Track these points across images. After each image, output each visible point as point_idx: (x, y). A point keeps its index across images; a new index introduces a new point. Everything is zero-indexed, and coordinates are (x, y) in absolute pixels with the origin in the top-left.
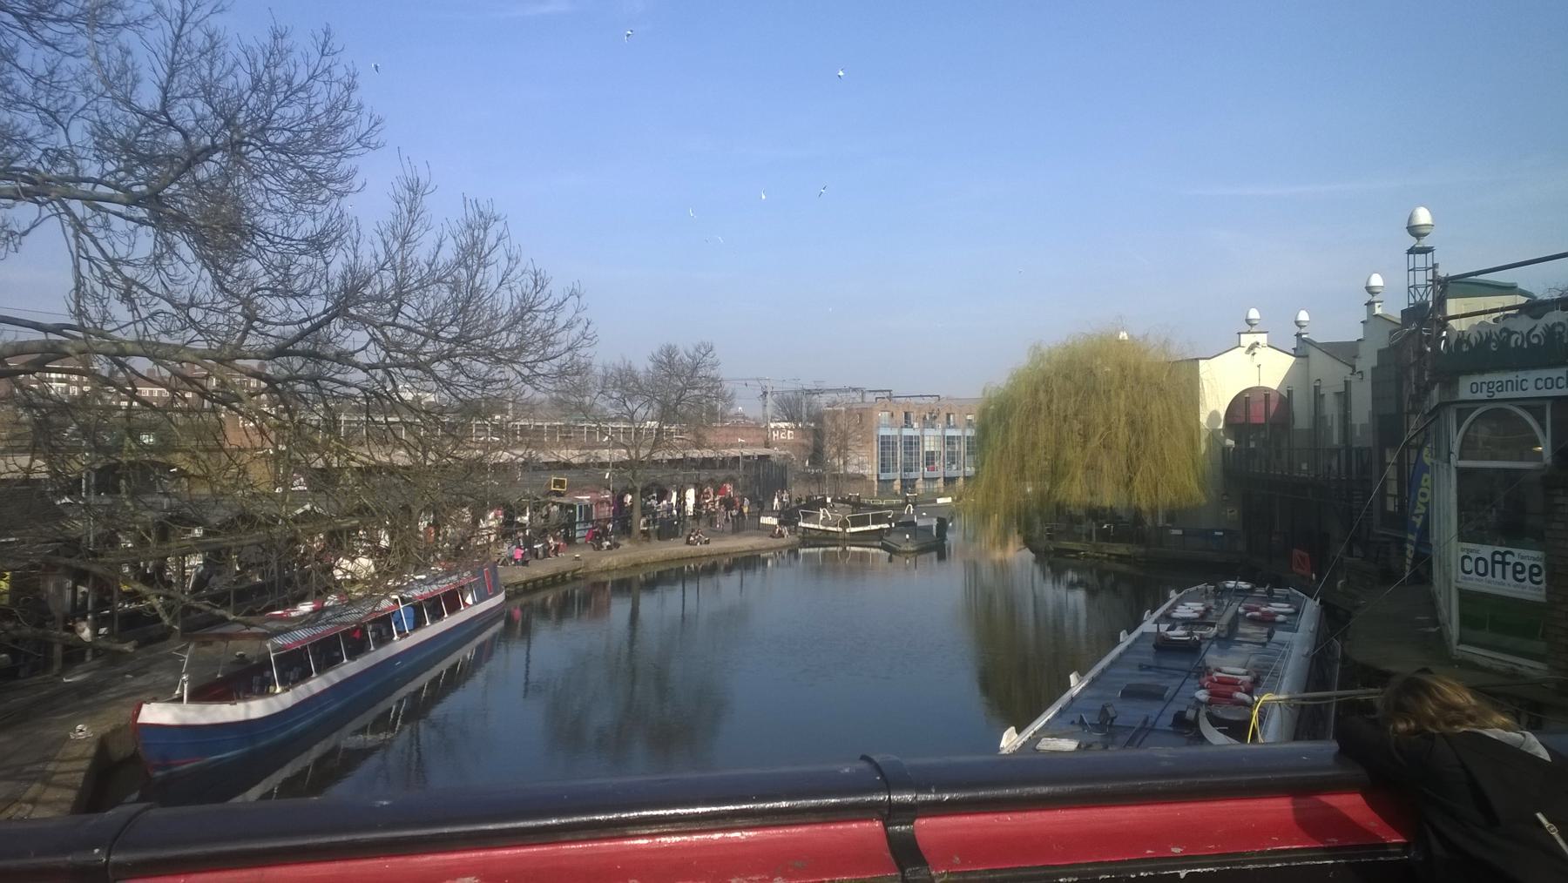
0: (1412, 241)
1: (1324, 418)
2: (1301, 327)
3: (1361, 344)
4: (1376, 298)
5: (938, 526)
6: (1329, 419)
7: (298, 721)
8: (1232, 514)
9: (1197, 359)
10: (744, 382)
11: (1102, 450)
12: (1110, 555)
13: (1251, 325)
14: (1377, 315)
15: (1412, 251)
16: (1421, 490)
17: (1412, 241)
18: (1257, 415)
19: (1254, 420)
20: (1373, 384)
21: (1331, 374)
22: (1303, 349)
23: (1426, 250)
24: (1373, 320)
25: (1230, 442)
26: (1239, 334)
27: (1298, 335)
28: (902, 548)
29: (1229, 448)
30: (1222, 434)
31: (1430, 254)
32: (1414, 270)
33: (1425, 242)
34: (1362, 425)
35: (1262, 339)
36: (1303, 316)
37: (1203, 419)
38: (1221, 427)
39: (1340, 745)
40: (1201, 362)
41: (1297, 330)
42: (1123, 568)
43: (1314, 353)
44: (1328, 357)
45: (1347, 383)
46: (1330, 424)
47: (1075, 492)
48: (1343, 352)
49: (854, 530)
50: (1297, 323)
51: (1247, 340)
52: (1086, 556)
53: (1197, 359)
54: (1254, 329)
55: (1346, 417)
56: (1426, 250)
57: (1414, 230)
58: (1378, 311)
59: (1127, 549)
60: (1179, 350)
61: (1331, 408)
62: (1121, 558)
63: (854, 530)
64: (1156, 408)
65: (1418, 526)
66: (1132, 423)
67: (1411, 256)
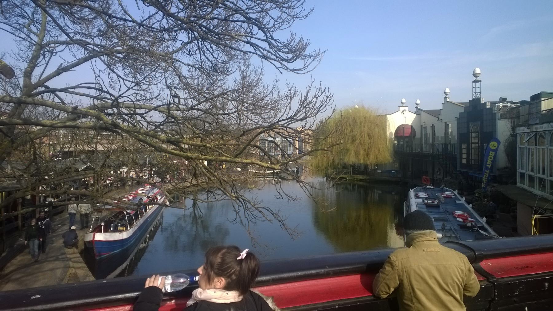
0: (474, 79)
2: (417, 105)
3: (442, 111)
4: (447, 96)
5: (297, 171)
6: (428, 135)
7: (132, 240)
8: (397, 165)
9: (386, 115)
11: (360, 144)
12: (357, 179)
13: (403, 104)
14: (448, 101)
15: (474, 82)
16: (490, 156)
17: (474, 79)
18: (407, 133)
19: (405, 135)
21: (429, 120)
22: (418, 111)
23: (478, 82)
24: (446, 103)
25: (396, 142)
26: (399, 107)
27: (417, 108)
28: (288, 178)
29: (396, 144)
30: (393, 139)
31: (479, 83)
32: (475, 87)
33: (478, 79)
35: (406, 108)
36: (418, 101)
37: (388, 134)
38: (393, 137)
40: (387, 116)
42: (361, 183)
43: (423, 113)
44: (428, 114)
46: (429, 136)
47: (351, 159)
48: (435, 113)
49: (268, 172)
50: (416, 103)
51: (402, 109)
52: (349, 180)
53: (386, 115)
54: (404, 105)
56: (478, 82)
57: (475, 75)
58: (448, 100)
59: (363, 177)
60: (380, 112)
61: (429, 131)
62: (361, 180)
63: (268, 172)
64: (376, 130)
65: (489, 168)
66: (369, 135)
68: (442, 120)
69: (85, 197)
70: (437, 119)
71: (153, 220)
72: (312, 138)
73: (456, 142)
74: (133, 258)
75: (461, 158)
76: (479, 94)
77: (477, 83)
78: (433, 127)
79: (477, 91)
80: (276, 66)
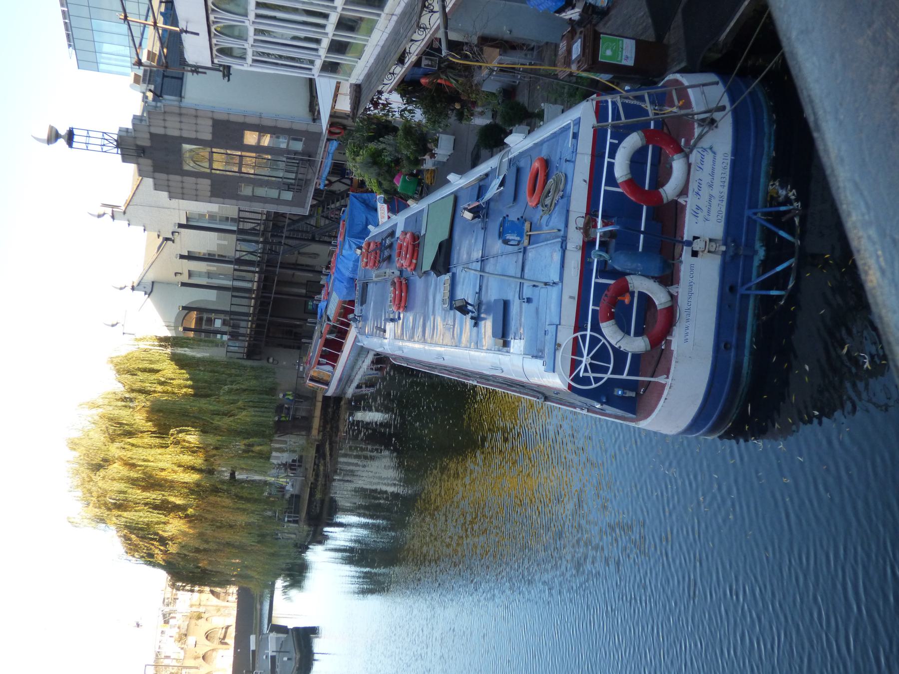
0: (62, 142)
17: (62, 142)
27: (133, 288)
31: (75, 132)
67: (74, 145)
70: (170, 243)
75: (278, 201)
77: (76, 138)
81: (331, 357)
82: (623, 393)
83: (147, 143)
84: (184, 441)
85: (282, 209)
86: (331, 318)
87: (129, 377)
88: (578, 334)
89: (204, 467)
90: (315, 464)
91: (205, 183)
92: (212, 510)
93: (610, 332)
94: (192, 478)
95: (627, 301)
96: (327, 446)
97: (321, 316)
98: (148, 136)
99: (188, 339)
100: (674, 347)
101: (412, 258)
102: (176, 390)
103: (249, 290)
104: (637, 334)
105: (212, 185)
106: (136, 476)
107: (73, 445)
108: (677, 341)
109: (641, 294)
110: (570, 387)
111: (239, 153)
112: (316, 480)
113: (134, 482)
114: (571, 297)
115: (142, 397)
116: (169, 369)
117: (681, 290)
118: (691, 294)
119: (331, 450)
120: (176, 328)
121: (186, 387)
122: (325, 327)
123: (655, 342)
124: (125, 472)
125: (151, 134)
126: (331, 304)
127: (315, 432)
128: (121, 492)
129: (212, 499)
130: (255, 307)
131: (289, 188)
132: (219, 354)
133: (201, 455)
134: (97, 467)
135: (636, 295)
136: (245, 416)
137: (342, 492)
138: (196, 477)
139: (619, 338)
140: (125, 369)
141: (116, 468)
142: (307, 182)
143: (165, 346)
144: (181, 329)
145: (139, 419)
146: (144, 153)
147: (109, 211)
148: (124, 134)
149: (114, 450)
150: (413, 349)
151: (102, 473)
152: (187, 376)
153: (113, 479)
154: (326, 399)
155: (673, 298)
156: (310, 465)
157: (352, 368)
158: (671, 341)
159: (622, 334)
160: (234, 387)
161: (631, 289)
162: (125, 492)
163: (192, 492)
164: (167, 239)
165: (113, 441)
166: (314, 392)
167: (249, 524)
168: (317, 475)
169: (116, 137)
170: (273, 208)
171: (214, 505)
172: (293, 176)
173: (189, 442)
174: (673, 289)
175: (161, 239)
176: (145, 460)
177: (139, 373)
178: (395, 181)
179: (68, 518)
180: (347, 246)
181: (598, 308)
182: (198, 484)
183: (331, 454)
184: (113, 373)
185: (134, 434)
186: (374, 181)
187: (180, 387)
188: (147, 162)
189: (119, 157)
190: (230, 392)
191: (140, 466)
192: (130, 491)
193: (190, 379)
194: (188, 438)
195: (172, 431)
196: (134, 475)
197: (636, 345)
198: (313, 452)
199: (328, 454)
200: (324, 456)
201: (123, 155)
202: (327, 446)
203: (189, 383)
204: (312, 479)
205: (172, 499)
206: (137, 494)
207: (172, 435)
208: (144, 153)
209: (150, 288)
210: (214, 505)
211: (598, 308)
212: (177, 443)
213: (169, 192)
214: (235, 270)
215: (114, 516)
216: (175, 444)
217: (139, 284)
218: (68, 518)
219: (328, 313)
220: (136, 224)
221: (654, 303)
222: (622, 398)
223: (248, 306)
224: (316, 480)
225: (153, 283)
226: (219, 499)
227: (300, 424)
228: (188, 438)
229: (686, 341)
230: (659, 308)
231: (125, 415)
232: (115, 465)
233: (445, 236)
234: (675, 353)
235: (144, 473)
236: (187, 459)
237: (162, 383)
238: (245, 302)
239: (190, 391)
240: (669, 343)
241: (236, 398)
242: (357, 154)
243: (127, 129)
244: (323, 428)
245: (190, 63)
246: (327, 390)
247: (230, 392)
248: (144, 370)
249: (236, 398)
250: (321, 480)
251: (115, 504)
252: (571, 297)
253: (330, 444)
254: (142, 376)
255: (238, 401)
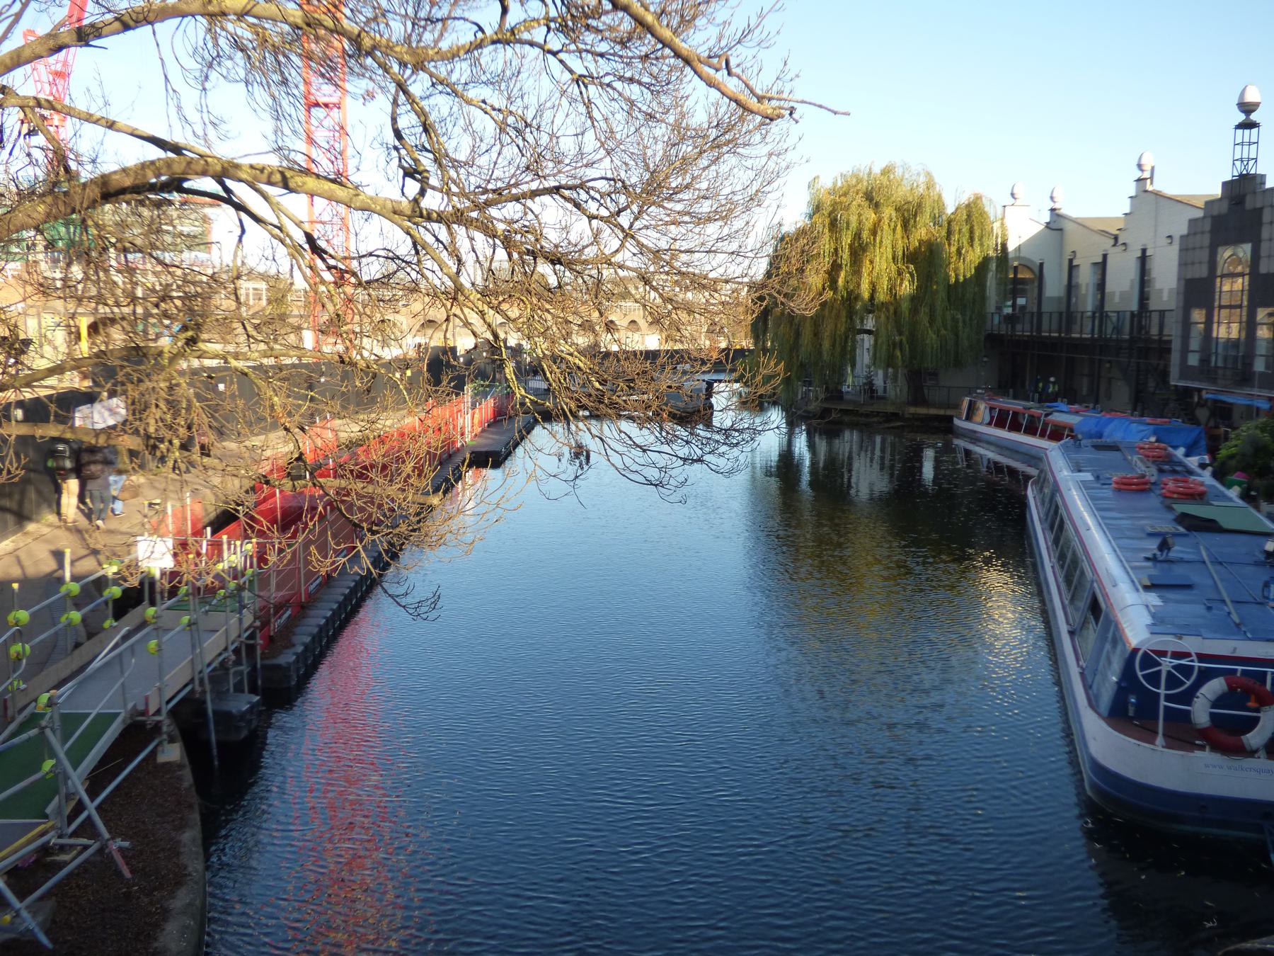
0: (1242, 117)
1: (1078, 286)
10: (1018, 202)
17: (1242, 117)
20: (1181, 250)
27: (1053, 210)
31: (1255, 131)
34: (1122, 294)
39: (121, 597)
41: (1051, 205)
45: (1105, 256)
55: (1071, 287)
61: (1086, 277)
67: (1240, 132)
68: (1124, 244)
69: (241, 813)
70: (1112, 242)
71: (87, 577)
72: (291, 320)
73: (1172, 305)
74: (210, 834)
75: (1185, 350)
76: (1251, 163)
77: (1247, 132)
78: (1102, 266)
79: (1245, 156)
80: (208, 190)
81: (1000, 420)
82: (1132, 703)
83: (1249, 204)
84: (902, 280)
85: (1175, 357)
86: (1050, 417)
87: (965, 217)
88: (1194, 657)
89: (876, 301)
90: (878, 412)
91: (1202, 272)
92: (833, 314)
93: (1215, 687)
94: (865, 290)
95: (1251, 704)
96: (899, 424)
97: (1049, 407)
98: (1259, 205)
99: (1007, 273)
100: (1198, 753)
101: (1179, 493)
102: (952, 266)
103: (1039, 329)
104: (1212, 715)
105: (1201, 280)
106: (864, 236)
107: (886, 171)
108: (1205, 757)
109: (1256, 720)
110: (1136, 651)
111: (1245, 303)
112: (862, 415)
113: (858, 235)
114: (1235, 649)
115: (944, 233)
116: (974, 256)
117: (1262, 762)
118: (1259, 771)
119: (898, 428)
120: (1018, 258)
121: (957, 275)
122: (1037, 412)
123: (1203, 733)
124: (868, 225)
125: (1261, 209)
126: (1064, 416)
127: (912, 410)
128: (848, 224)
129: (844, 313)
130: (1081, 339)
131: (1205, 361)
132: (991, 306)
133: (888, 297)
134: (870, 197)
135: (1255, 714)
136: (931, 338)
137: (849, 440)
138: (866, 295)
139: (1209, 696)
140: (973, 213)
141: (871, 216)
142: (1213, 381)
143: (996, 250)
144: (1016, 264)
145: (921, 232)
146: (1236, 204)
147: (1147, 175)
148: (1258, 181)
149: (888, 212)
150: (1074, 501)
151: (866, 204)
152: (968, 276)
153: (860, 215)
154: (950, 419)
155: (1252, 753)
156: (877, 407)
157: (989, 443)
158: (1204, 750)
159: (1213, 699)
160: (961, 324)
161: (1264, 708)
162: (848, 228)
163: (850, 293)
164: (1116, 238)
165: (897, 210)
166: (957, 406)
167: (820, 353)
168: (867, 416)
169: (1253, 172)
170: (1176, 345)
171: (838, 317)
172: (1220, 364)
173: (901, 284)
174: (1262, 753)
175: (1117, 232)
176: (881, 242)
177: (968, 227)
178: (1238, 473)
179: (818, 177)
180: (1142, 428)
181: (1239, 674)
182: (858, 297)
183: (888, 428)
184: (964, 200)
185: (906, 231)
186: (1233, 450)
187: (956, 270)
188: (1224, 208)
189: (1229, 178)
190: (955, 320)
191: (874, 239)
192: (849, 232)
193: (965, 279)
194: (906, 283)
195: (912, 267)
196: (865, 235)
197: (1201, 712)
198: (891, 409)
199: (892, 425)
200: (888, 421)
201: (1232, 182)
202: (899, 424)
203: (961, 278)
204: (862, 410)
205: (843, 274)
206: (847, 240)
207: (908, 268)
208: (1236, 204)
209: (1057, 224)
210: (838, 317)
211: (1239, 674)
212: (900, 273)
213: (1188, 235)
214: (1033, 313)
215: (822, 221)
216: (898, 271)
217: (1059, 215)
218: (818, 177)
219: (1055, 414)
220: (1132, 205)
221: (1249, 732)
222: (1126, 703)
223: (1049, 330)
224: (862, 415)
225: (1061, 230)
226: (844, 320)
227: (918, 397)
228: (906, 283)
229: (1207, 766)
230: (1243, 737)
231: (924, 221)
232: (873, 215)
233: (1226, 524)
234: (1192, 754)
235: (867, 244)
236: (884, 284)
237: (959, 252)
238: (1055, 326)
239: (953, 280)
240: (1202, 748)
241: (949, 327)
242: (1263, 430)
243: (1264, 183)
244: (916, 418)
245: (304, 195)
246: (960, 419)
247: (955, 320)
248: (971, 232)
249: (949, 327)
250: (863, 420)
251: (836, 220)
252: (1235, 649)
253: (902, 426)
254: (965, 229)
255: (946, 329)
